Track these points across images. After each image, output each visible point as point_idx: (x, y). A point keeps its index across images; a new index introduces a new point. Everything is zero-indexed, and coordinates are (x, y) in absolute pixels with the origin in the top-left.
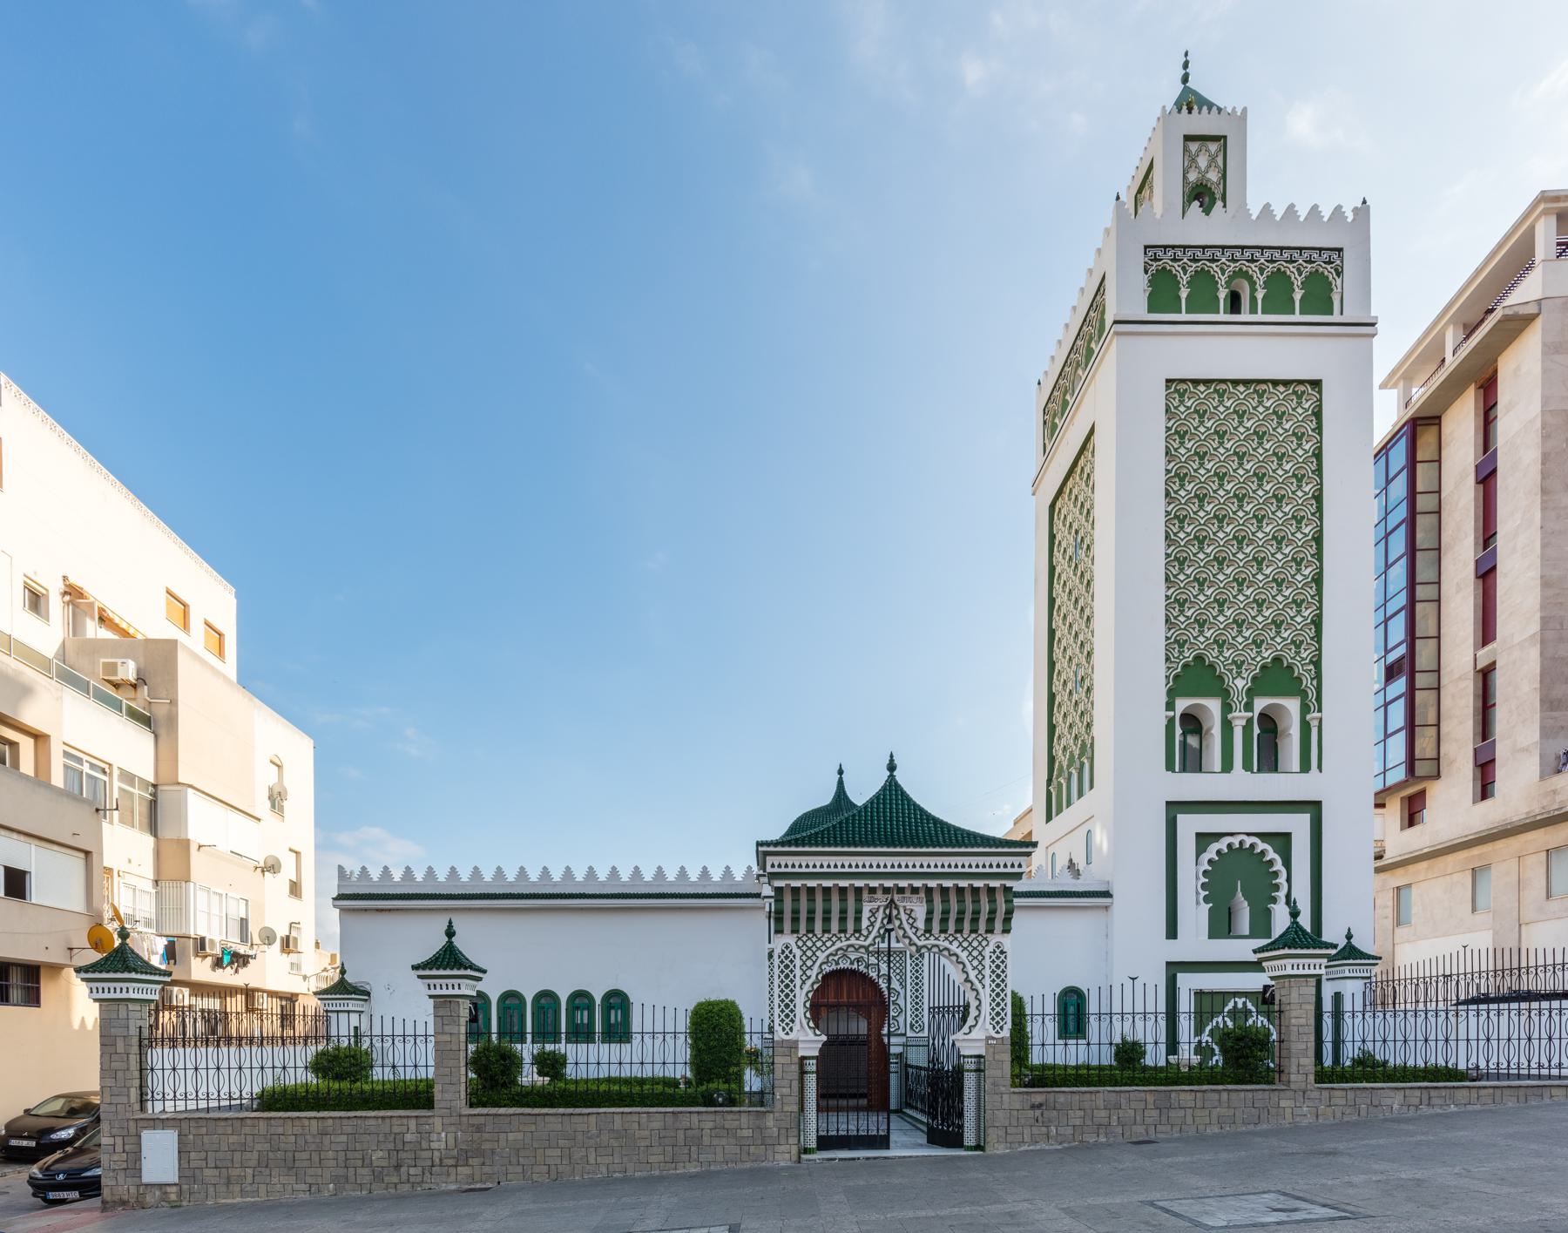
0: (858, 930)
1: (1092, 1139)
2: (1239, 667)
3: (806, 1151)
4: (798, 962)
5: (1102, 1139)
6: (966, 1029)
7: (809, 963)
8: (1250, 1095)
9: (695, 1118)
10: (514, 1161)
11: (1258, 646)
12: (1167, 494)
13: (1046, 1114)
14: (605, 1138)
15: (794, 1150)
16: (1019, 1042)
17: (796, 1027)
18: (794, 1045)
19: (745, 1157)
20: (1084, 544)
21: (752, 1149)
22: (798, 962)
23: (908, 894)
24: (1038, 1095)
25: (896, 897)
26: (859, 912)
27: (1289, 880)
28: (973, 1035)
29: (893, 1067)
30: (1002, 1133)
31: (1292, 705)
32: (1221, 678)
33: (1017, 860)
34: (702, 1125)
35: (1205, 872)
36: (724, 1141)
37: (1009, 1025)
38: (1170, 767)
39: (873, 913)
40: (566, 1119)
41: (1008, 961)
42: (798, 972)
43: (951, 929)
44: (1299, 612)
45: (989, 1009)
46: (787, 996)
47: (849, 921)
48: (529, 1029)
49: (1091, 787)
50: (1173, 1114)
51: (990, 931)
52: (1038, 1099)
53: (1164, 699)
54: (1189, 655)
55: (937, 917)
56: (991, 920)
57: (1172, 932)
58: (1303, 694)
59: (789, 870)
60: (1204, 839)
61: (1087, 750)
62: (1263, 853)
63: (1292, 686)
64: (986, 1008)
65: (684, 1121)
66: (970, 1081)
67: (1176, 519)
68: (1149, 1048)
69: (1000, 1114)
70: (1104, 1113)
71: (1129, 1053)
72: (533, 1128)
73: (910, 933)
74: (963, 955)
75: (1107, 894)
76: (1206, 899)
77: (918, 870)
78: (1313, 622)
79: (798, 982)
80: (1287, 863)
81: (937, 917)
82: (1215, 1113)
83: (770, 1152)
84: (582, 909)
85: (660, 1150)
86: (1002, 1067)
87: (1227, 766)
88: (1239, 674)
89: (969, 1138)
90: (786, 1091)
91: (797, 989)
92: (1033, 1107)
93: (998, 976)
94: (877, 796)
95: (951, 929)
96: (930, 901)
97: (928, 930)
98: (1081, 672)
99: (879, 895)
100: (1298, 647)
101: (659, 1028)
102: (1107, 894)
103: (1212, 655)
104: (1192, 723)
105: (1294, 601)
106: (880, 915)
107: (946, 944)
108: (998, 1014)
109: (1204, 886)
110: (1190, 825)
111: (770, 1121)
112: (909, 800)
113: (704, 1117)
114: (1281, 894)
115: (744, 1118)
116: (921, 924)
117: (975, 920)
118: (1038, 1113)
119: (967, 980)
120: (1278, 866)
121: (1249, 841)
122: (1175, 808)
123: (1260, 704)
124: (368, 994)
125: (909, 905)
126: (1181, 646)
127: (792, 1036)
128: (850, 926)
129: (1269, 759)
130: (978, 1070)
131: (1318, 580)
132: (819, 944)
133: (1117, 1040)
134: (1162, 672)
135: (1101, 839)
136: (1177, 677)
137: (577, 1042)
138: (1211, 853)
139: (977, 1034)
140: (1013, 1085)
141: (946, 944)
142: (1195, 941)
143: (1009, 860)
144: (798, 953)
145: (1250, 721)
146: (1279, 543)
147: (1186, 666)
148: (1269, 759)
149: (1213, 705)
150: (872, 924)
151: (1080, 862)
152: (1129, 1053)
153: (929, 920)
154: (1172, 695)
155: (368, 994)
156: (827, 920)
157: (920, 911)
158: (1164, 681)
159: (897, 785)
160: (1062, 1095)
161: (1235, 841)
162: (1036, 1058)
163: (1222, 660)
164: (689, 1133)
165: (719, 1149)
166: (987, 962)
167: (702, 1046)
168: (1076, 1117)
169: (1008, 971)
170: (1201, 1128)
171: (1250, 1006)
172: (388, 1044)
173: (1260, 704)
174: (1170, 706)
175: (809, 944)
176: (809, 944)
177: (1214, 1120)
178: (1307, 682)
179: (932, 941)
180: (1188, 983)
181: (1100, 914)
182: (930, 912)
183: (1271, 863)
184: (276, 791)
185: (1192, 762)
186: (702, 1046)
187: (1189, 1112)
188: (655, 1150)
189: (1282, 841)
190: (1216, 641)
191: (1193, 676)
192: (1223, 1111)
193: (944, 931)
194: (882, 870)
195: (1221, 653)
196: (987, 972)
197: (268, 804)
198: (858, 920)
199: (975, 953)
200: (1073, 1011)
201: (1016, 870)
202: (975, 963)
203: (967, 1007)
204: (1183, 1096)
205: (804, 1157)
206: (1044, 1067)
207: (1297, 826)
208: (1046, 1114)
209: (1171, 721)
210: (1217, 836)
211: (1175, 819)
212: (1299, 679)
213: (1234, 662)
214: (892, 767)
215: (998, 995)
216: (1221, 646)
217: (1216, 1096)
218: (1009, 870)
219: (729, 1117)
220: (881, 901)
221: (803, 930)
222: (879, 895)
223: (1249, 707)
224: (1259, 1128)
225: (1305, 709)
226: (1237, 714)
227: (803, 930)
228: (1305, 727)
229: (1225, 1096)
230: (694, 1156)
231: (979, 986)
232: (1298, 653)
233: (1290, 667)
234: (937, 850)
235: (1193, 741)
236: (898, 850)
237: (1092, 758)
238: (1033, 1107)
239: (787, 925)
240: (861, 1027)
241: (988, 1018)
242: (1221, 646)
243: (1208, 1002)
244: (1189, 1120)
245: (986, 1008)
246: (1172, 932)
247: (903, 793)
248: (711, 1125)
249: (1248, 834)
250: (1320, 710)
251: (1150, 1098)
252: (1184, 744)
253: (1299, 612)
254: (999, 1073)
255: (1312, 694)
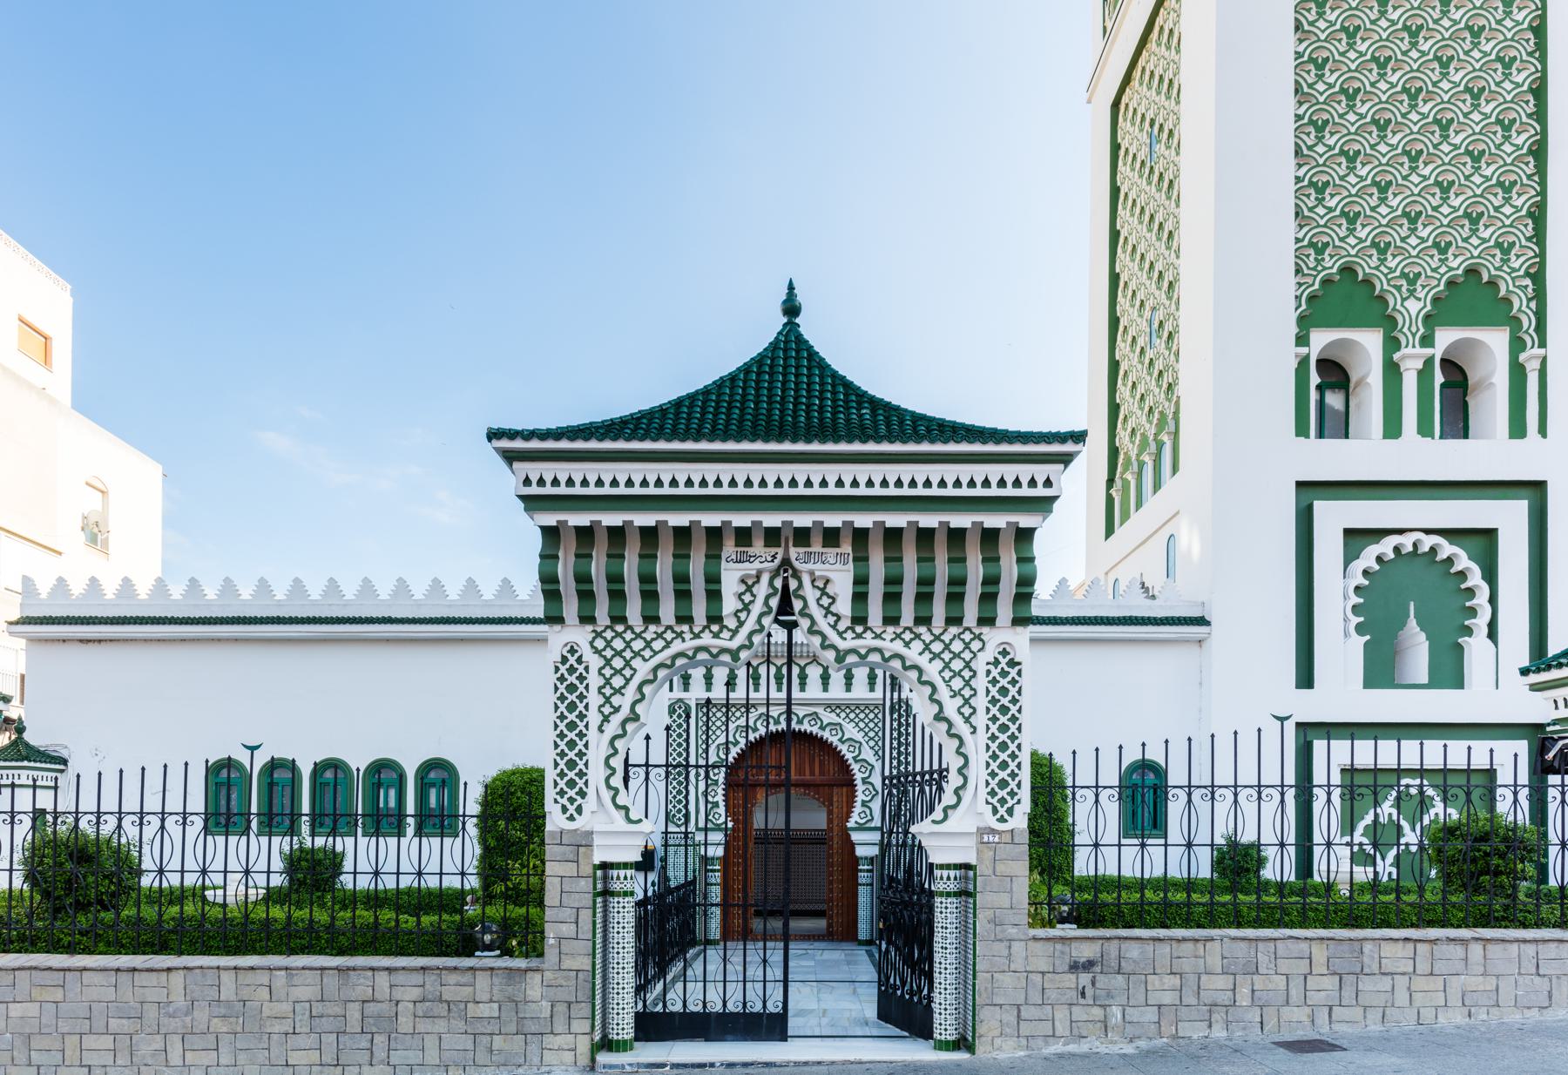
0: (715, 618)
1: (1196, 1032)
2: (1412, 282)
3: (607, 1044)
4: (594, 680)
5: (1219, 1033)
6: (938, 814)
7: (617, 682)
8: (1530, 950)
9: (382, 980)
10: (21, 1057)
11: (1443, 251)
12: (1298, 27)
13: (1102, 981)
14: (201, 1015)
15: (584, 1045)
16: (1049, 838)
17: (589, 804)
18: (584, 842)
19: (482, 1057)
20: (1164, 133)
21: (498, 1042)
22: (594, 680)
23: (817, 547)
24: (1086, 943)
25: (794, 552)
26: (713, 580)
27: (1493, 600)
28: (952, 824)
29: (863, 877)
30: (1010, 1017)
31: (1496, 340)
32: (1382, 299)
33: (1041, 471)
34: (398, 994)
35: (1357, 588)
36: (441, 1026)
37: (1025, 807)
38: (1302, 430)
39: (748, 585)
40: (124, 978)
41: (1024, 681)
42: (594, 699)
43: (907, 618)
44: (1507, 200)
45: (984, 775)
46: (571, 744)
47: (697, 600)
48: (306, 807)
49: (1175, 469)
50: (1366, 984)
51: (987, 620)
52: (1086, 952)
53: (1293, 330)
54: (1332, 265)
55: (876, 590)
56: (988, 598)
57: (1306, 679)
58: (1515, 323)
59: (563, 490)
60: (1356, 538)
61: (1169, 423)
62: (1450, 561)
63: (1496, 310)
64: (977, 772)
65: (361, 986)
66: (945, 915)
67: (1311, 63)
68: (1270, 853)
69: (1007, 980)
70: (1223, 982)
71: (1237, 861)
72: (58, 995)
73: (823, 624)
74: (933, 670)
75: (1201, 621)
76: (1360, 629)
77: (832, 490)
78: (1530, 214)
79: (594, 718)
80: (1491, 576)
81: (876, 590)
82: (1456, 984)
83: (533, 1048)
84: (388, 640)
85: (312, 1040)
86: (1011, 884)
87: (1393, 428)
88: (1412, 293)
89: (945, 1025)
90: (568, 930)
91: (592, 734)
92: (1075, 967)
93: (1004, 710)
94: (759, 360)
95: (907, 618)
96: (861, 558)
97: (860, 619)
98: (1159, 315)
99: (758, 547)
100: (1506, 251)
101: (1201, 777)
102: (1201, 621)
103: (1367, 266)
104: (1335, 373)
105: (1500, 184)
106: (762, 589)
107: (898, 646)
108: (1003, 784)
109: (1356, 609)
110: (1332, 517)
111: (534, 987)
112: (823, 366)
113: (400, 978)
114: (1481, 622)
115: (483, 980)
116: (844, 607)
117: (955, 598)
118: (1085, 979)
119: (939, 717)
120: (1476, 579)
121: (1428, 541)
122: (1309, 489)
123: (1445, 338)
124: (65, 762)
125: (820, 569)
126: (1320, 251)
127: (581, 823)
128: (699, 610)
129: (1456, 417)
130: (965, 893)
131: (1539, 152)
132: (638, 645)
133: (1219, 840)
134: (1292, 291)
135: (1190, 541)
136: (1312, 298)
137: (377, 833)
138: (1368, 557)
139: (957, 822)
140: (1036, 920)
141: (898, 646)
142: (1342, 690)
143: (1025, 471)
144: (595, 662)
145: (1429, 362)
146: (1476, 97)
147: (1326, 282)
148: (1457, 421)
149: (1370, 341)
150: (746, 608)
151: (1156, 580)
152: (1237, 861)
153: (860, 598)
154: (1305, 325)
155: (65, 762)
156: (650, 595)
157: (842, 584)
158: (1293, 304)
159: (799, 339)
160: (1137, 946)
161: (1407, 541)
162: (1082, 865)
163: (1382, 273)
164: (371, 1008)
165: (431, 1042)
166: (981, 683)
167: (492, 843)
168: (1163, 989)
169: (1024, 700)
170: (1428, 1015)
171: (1430, 792)
172: (150, 830)
173: (1445, 338)
174: (1302, 340)
175: (618, 644)
176: (618, 644)
177: (1455, 1000)
178: (1521, 304)
179: (869, 641)
180: (1331, 758)
181: (1187, 655)
182: (861, 581)
183: (1462, 575)
184: (92, 520)
185: (1336, 426)
186: (492, 843)
187: (1402, 982)
188: (301, 1041)
189: (1484, 541)
190: (1374, 245)
191: (1339, 297)
192: (1475, 982)
193: (891, 620)
194: (756, 491)
195: (1383, 261)
196: (981, 702)
197: (82, 537)
198: (714, 596)
199: (957, 665)
200: (1145, 796)
201: (1040, 491)
202: (957, 683)
203: (942, 773)
204: (1388, 950)
205: (603, 1058)
206: (1098, 883)
207: (1510, 518)
208: (1102, 981)
209: (1303, 363)
210: (1379, 534)
211: (1310, 508)
212: (1507, 301)
213: (1404, 275)
214: (791, 309)
215: (1003, 746)
216: (1383, 252)
217: (1458, 951)
218: (1025, 491)
219: (453, 978)
220: (763, 558)
221: (603, 618)
222: (758, 547)
223: (1427, 341)
224: (1550, 1016)
225: (1517, 344)
226: (1410, 350)
227: (603, 618)
228: (1518, 372)
229: (1476, 950)
230: (380, 1054)
231: (962, 728)
232: (1505, 261)
233: (1492, 283)
234: (871, 447)
235: (1334, 400)
236: (787, 446)
237: (1176, 434)
238: (1075, 967)
239: (571, 608)
240: (811, 818)
241: (983, 792)
242: (1383, 252)
243: (1361, 786)
244: (1402, 997)
245: (977, 772)
246: (1306, 679)
247: (809, 348)
248: (415, 993)
249: (1428, 532)
250: (1543, 344)
251: (1320, 953)
252: (1321, 403)
253: (1507, 200)
254: (1004, 900)
255: (1528, 322)
